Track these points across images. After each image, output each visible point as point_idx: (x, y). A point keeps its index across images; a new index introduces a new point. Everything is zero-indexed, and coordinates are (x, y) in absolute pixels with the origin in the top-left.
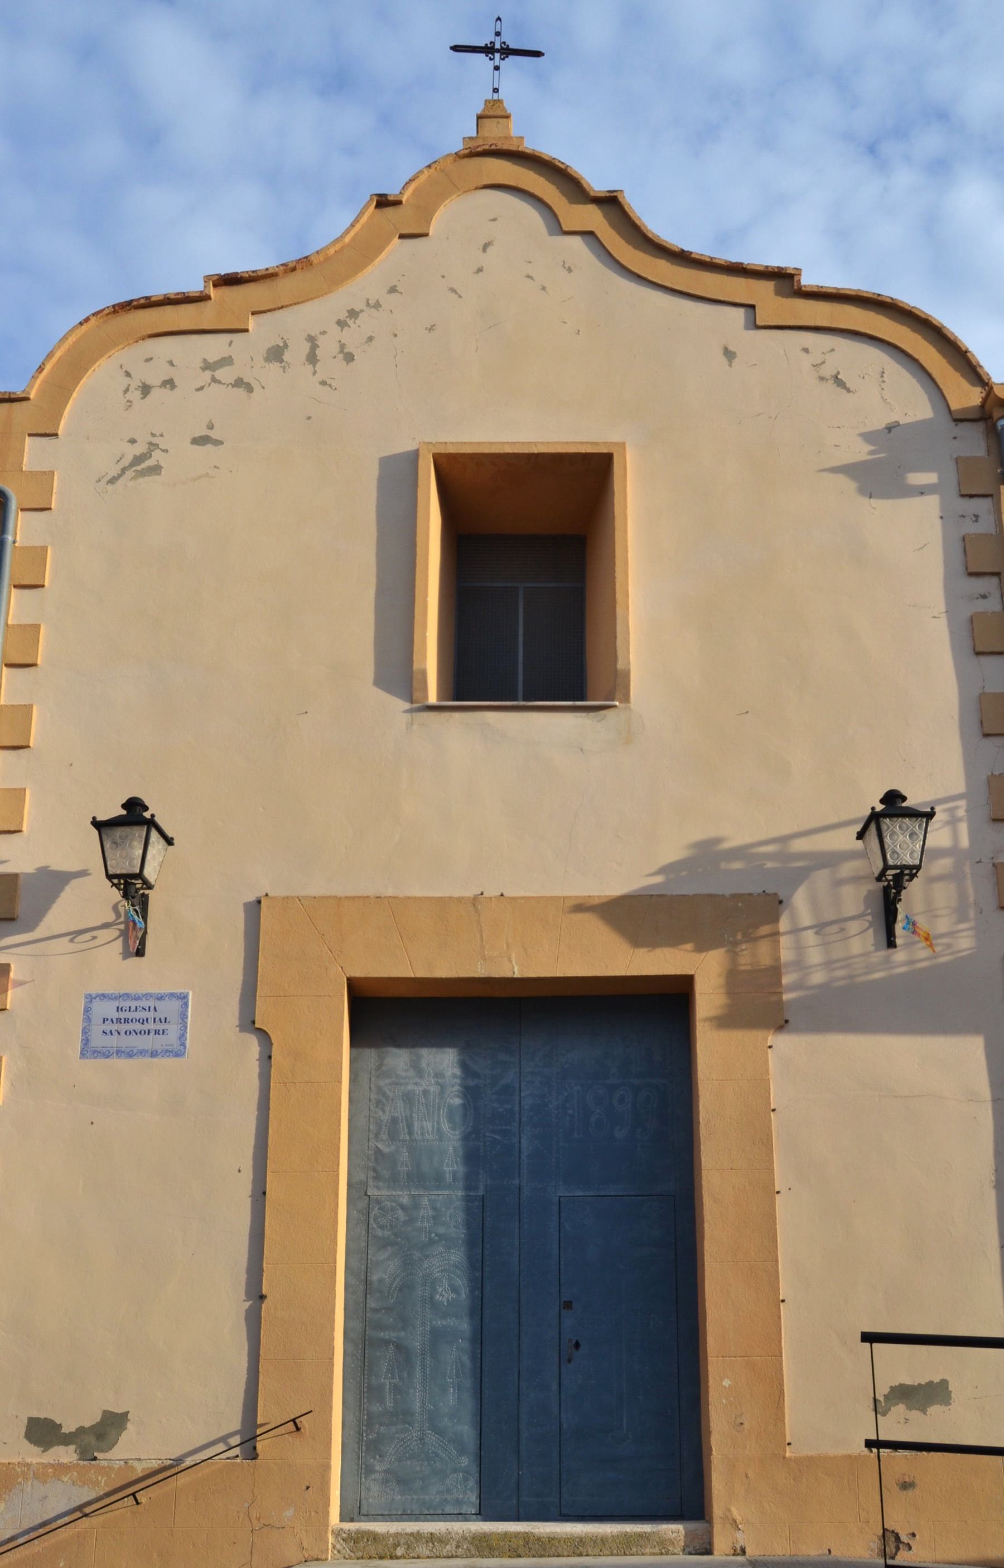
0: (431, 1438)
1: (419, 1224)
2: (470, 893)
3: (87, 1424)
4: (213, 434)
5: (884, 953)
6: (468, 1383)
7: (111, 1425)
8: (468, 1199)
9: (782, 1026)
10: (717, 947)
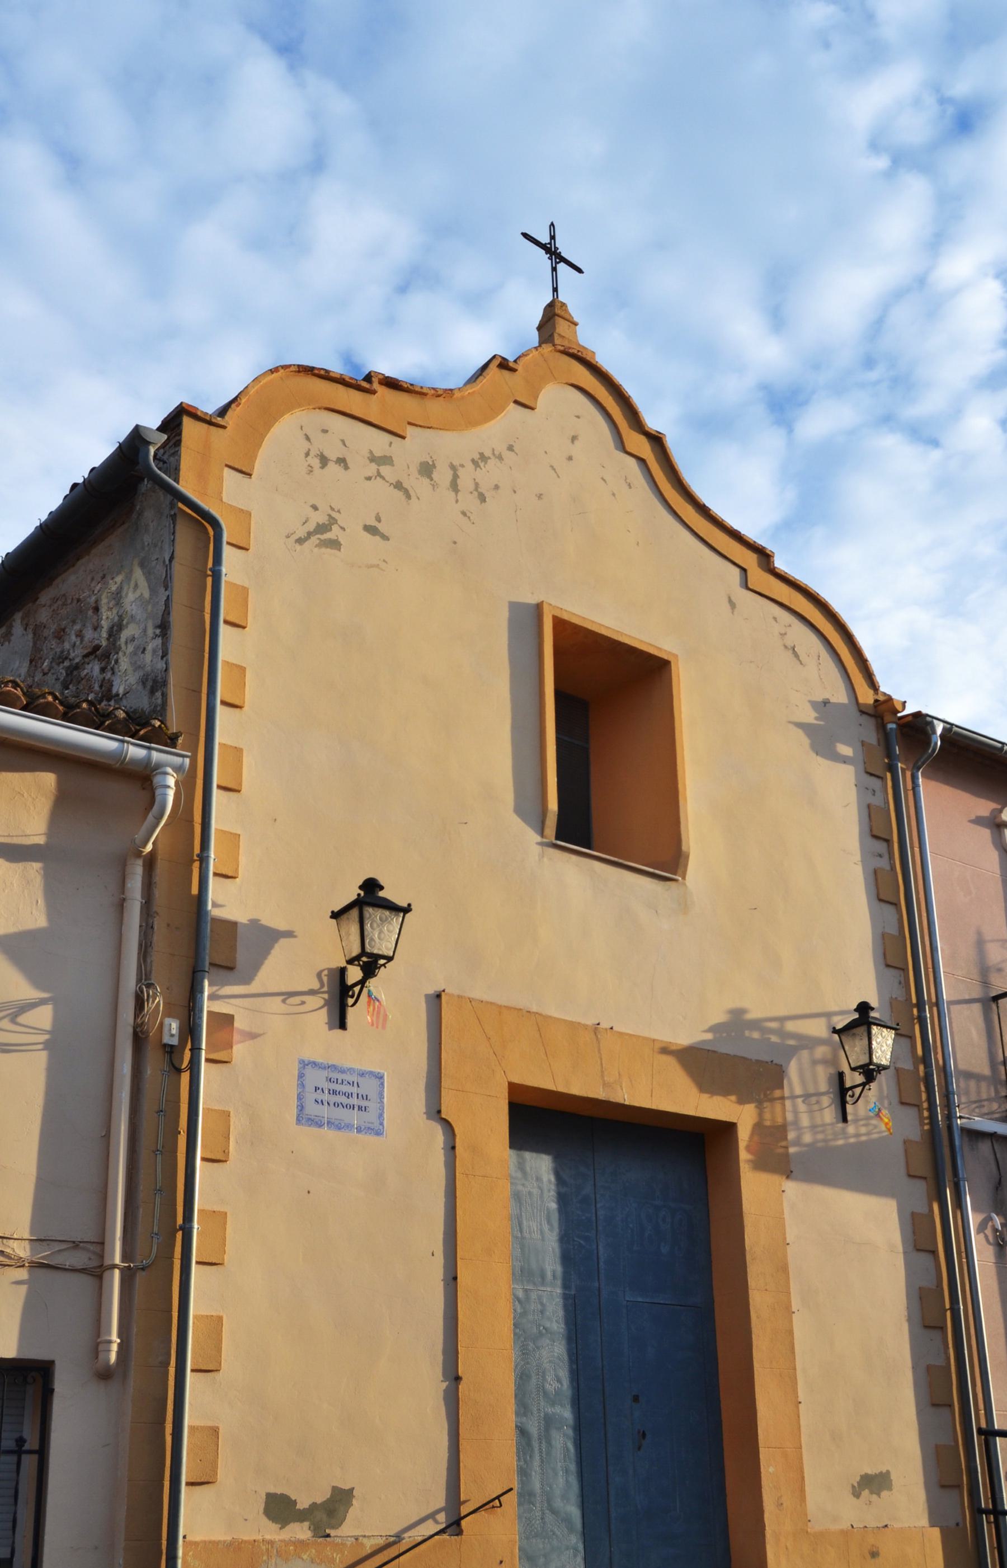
0: (549, 1517)
1: (531, 1317)
2: (590, 1021)
3: (319, 1500)
4: (379, 526)
5: (841, 1125)
6: (573, 1467)
7: (339, 1501)
8: (565, 1297)
9: (789, 1175)
10: (749, 1103)
